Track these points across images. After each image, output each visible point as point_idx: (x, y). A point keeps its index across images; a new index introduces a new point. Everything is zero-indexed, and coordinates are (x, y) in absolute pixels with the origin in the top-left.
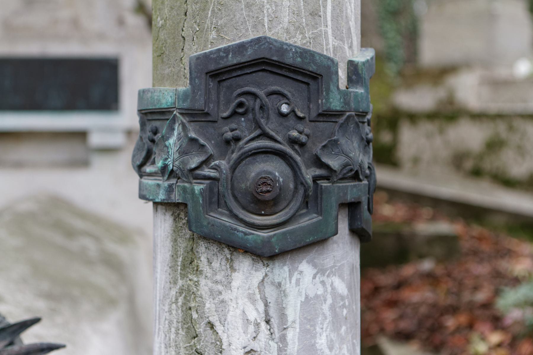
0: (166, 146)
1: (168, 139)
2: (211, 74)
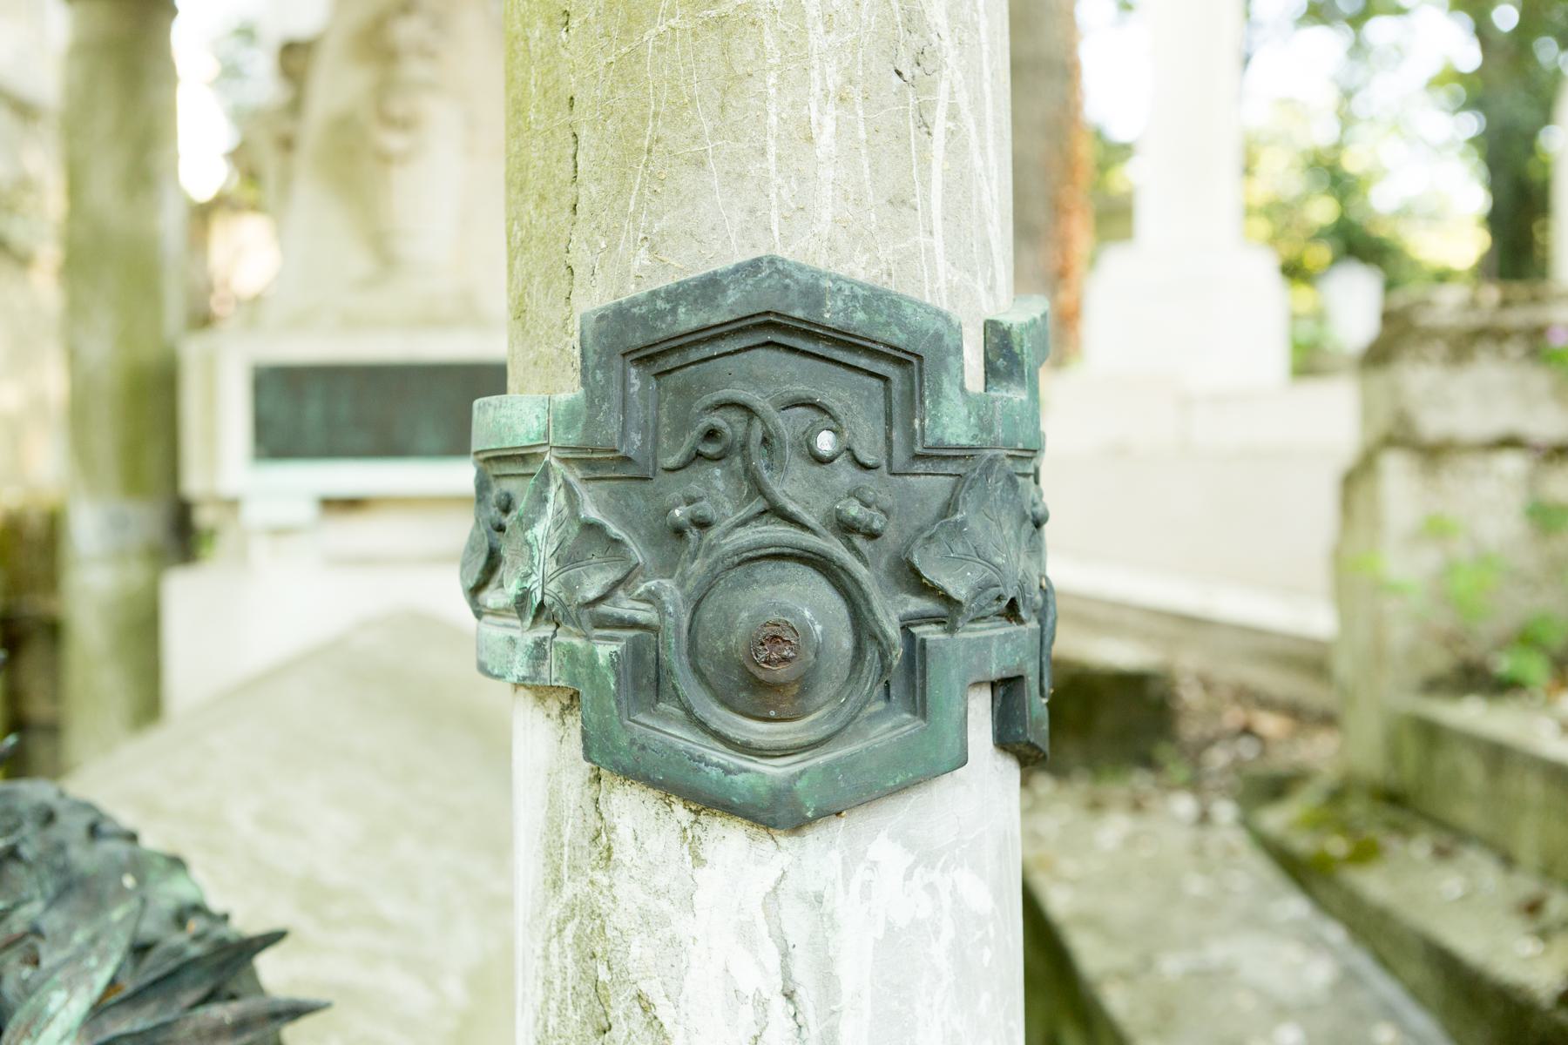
0: (527, 543)
1: (532, 523)
2: (635, 356)
